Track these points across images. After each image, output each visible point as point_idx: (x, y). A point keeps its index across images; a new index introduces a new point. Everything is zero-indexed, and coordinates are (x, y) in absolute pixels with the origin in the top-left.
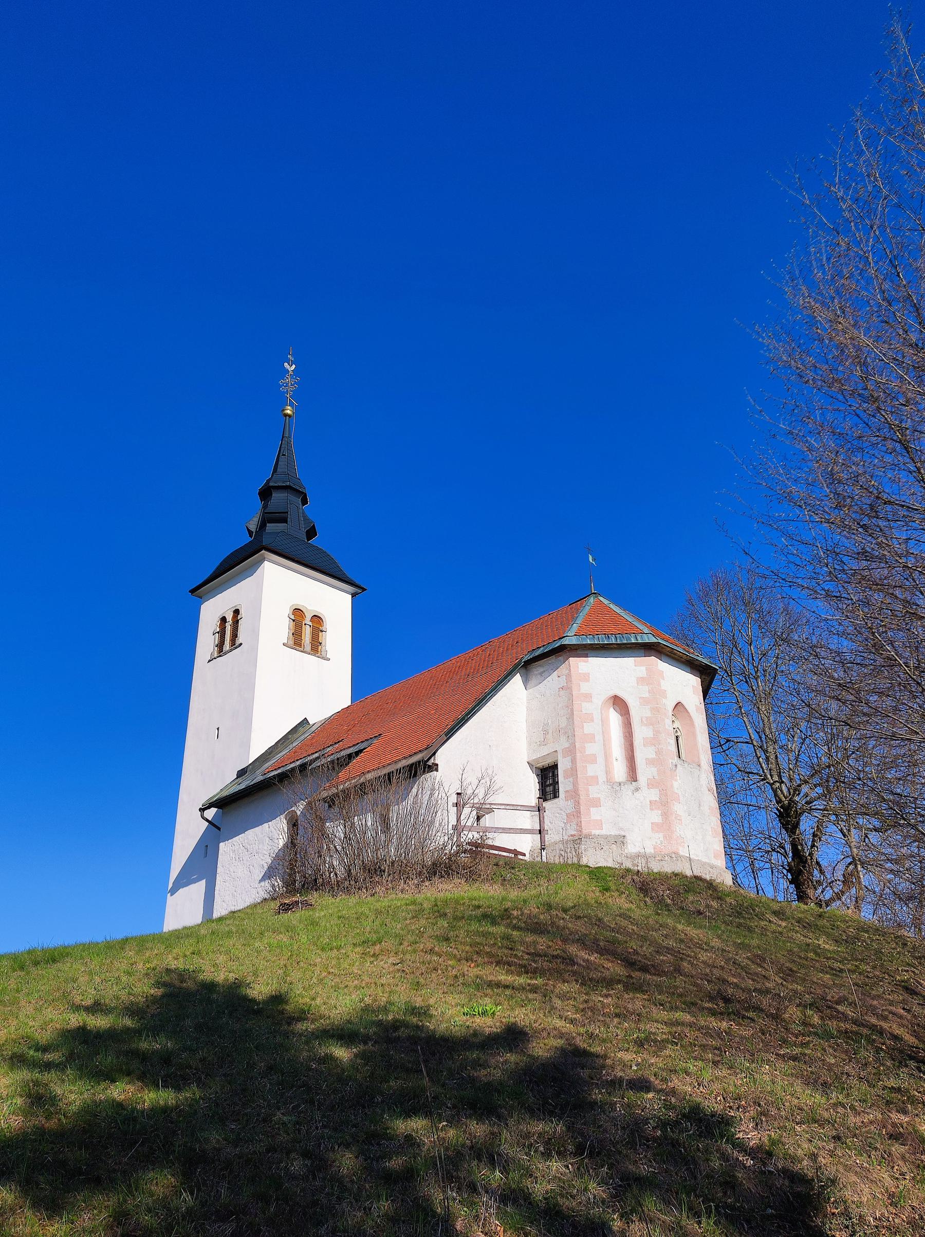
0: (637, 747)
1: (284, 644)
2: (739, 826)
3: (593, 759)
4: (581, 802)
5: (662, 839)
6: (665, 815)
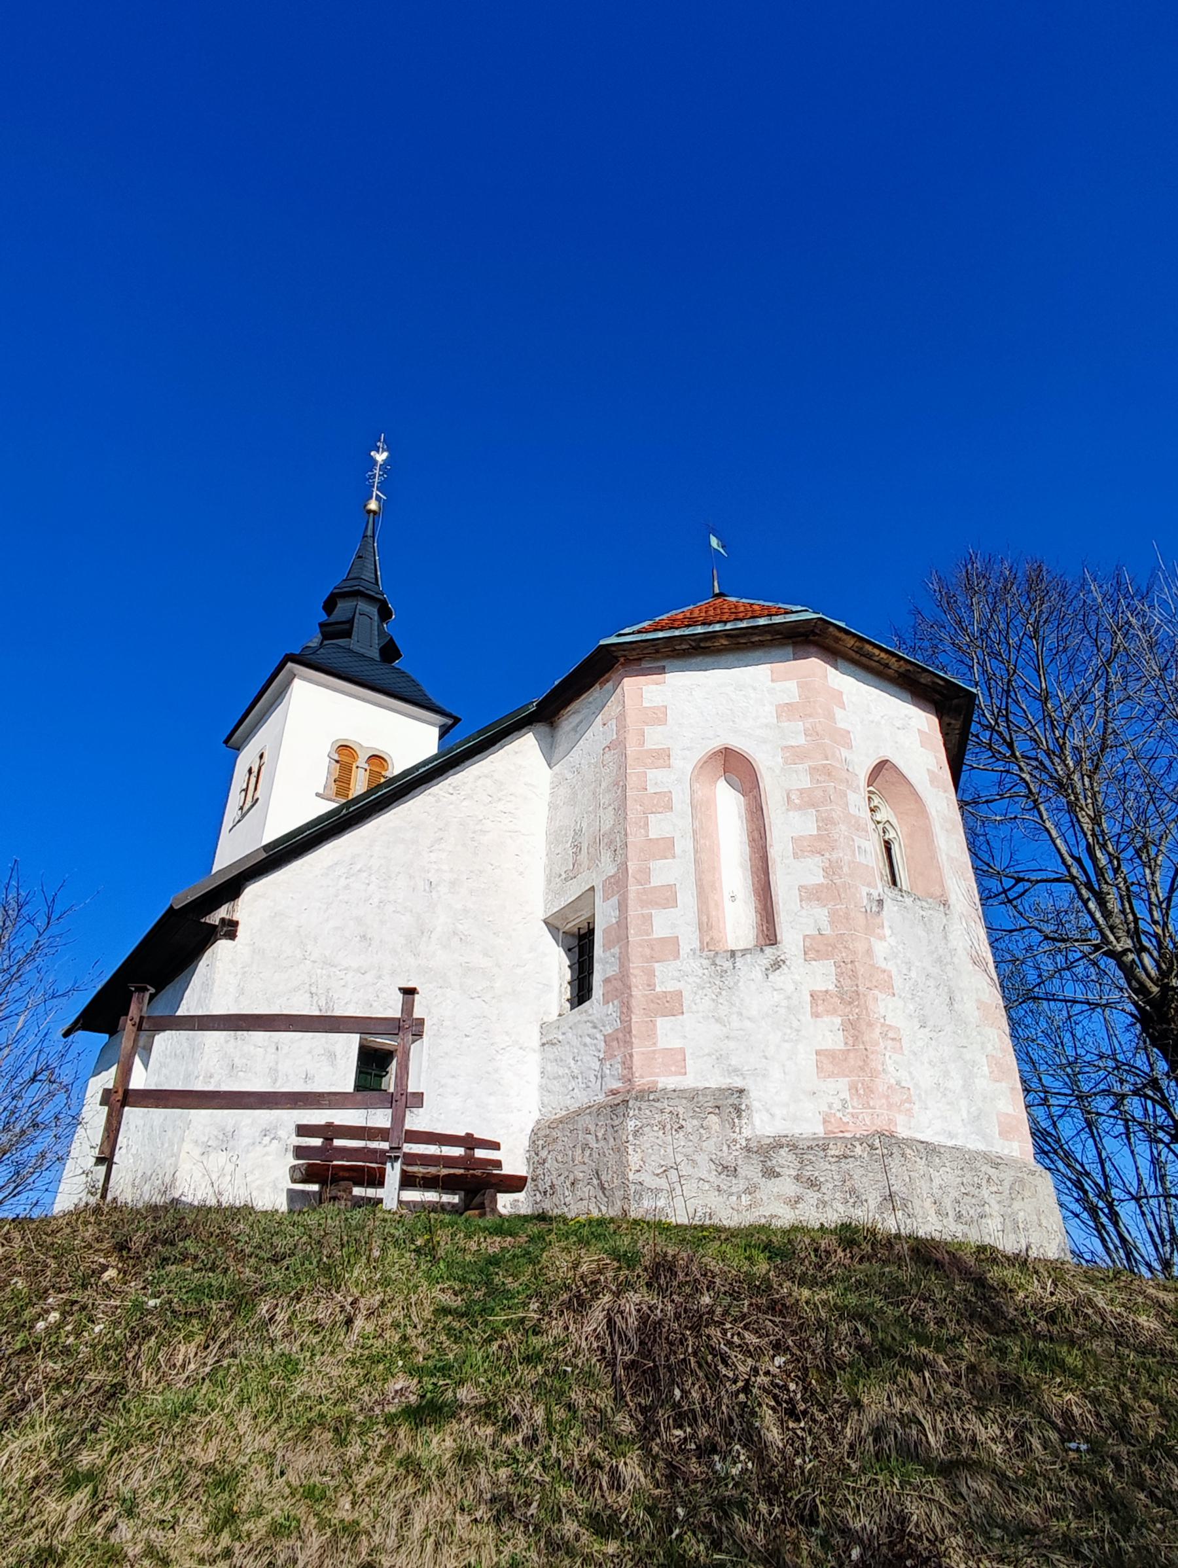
0: (778, 860)
1: (318, 795)
2: (1056, 1046)
3: (667, 898)
4: (634, 1003)
5: (845, 1095)
6: (854, 1028)
